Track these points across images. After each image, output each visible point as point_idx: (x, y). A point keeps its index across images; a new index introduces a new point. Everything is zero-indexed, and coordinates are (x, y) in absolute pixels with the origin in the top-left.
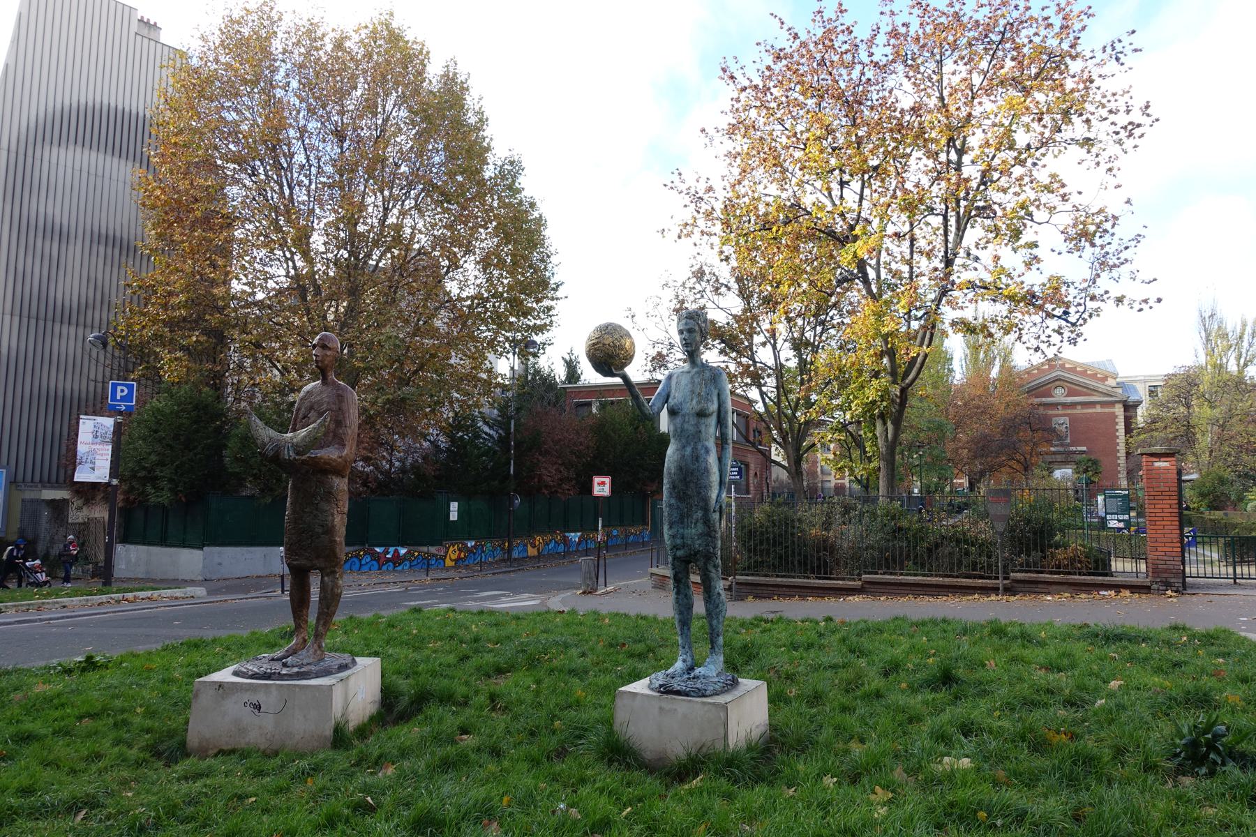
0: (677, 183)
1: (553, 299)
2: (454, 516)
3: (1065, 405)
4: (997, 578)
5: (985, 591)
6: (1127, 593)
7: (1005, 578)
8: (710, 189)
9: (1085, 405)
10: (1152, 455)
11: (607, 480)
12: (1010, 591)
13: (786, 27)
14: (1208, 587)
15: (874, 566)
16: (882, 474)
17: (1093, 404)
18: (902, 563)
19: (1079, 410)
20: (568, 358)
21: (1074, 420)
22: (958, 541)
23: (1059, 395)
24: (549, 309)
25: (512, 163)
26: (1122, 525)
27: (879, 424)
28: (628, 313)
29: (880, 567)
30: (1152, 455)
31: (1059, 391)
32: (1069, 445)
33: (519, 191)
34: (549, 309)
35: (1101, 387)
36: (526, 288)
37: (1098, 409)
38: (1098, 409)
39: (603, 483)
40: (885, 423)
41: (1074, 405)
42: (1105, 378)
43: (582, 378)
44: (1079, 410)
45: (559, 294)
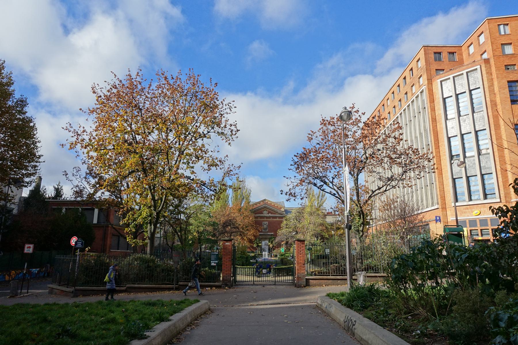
0: (69, 127)
1: (37, 162)
2: (487, 280)
3: (267, 217)
4: (173, 284)
5: (169, 289)
6: (214, 288)
7: (176, 284)
8: (84, 131)
9: (273, 217)
10: (225, 240)
11: (32, 246)
12: (177, 289)
13: (117, 78)
14: (240, 284)
15: (134, 282)
16: (149, 245)
17: (276, 217)
18: (144, 280)
19: (271, 219)
20: (57, 187)
21: (270, 223)
22: (168, 271)
23: (265, 214)
24: (35, 166)
25: (22, 101)
26: (215, 264)
27: (149, 225)
28: (64, 173)
29: (137, 282)
30: (225, 240)
31: (265, 212)
32: (268, 232)
33: (25, 113)
34: (35, 166)
35: (279, 212)
36: (24, 156)
37: (278, 219)
38: (278, 219)
39: (30, 247)
40: (151, 225)
41: (269, 217)
42: (281, 208)
43: (63, 197)
44: (271, 219)
45: (40, 160)
